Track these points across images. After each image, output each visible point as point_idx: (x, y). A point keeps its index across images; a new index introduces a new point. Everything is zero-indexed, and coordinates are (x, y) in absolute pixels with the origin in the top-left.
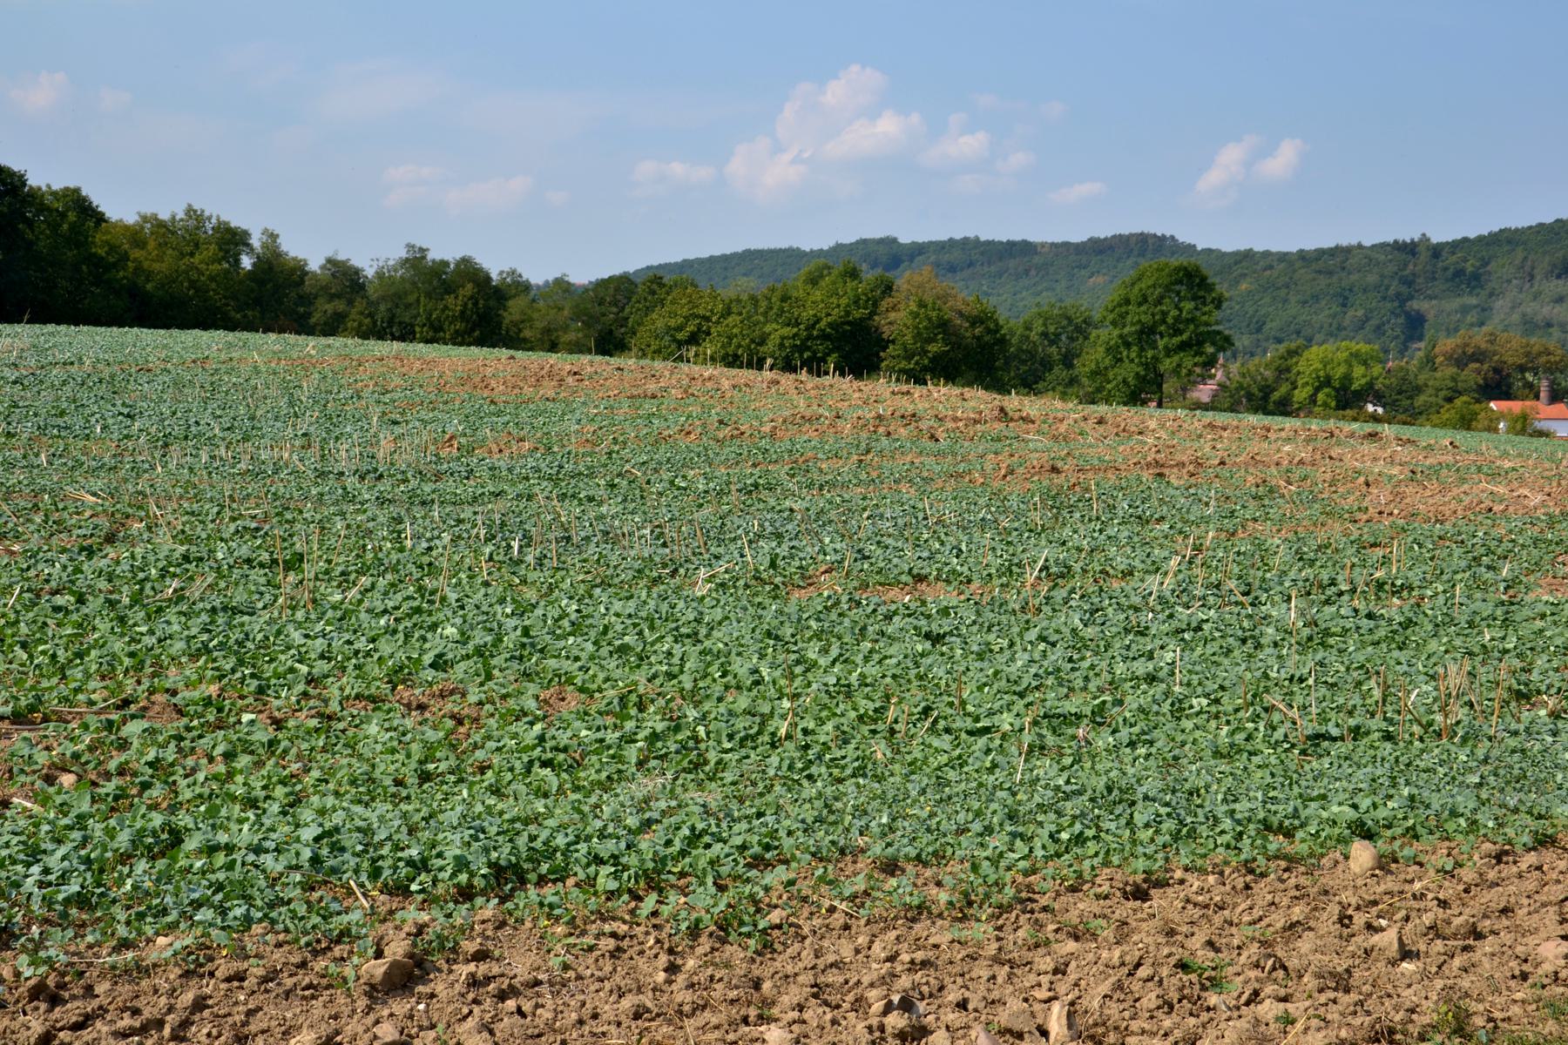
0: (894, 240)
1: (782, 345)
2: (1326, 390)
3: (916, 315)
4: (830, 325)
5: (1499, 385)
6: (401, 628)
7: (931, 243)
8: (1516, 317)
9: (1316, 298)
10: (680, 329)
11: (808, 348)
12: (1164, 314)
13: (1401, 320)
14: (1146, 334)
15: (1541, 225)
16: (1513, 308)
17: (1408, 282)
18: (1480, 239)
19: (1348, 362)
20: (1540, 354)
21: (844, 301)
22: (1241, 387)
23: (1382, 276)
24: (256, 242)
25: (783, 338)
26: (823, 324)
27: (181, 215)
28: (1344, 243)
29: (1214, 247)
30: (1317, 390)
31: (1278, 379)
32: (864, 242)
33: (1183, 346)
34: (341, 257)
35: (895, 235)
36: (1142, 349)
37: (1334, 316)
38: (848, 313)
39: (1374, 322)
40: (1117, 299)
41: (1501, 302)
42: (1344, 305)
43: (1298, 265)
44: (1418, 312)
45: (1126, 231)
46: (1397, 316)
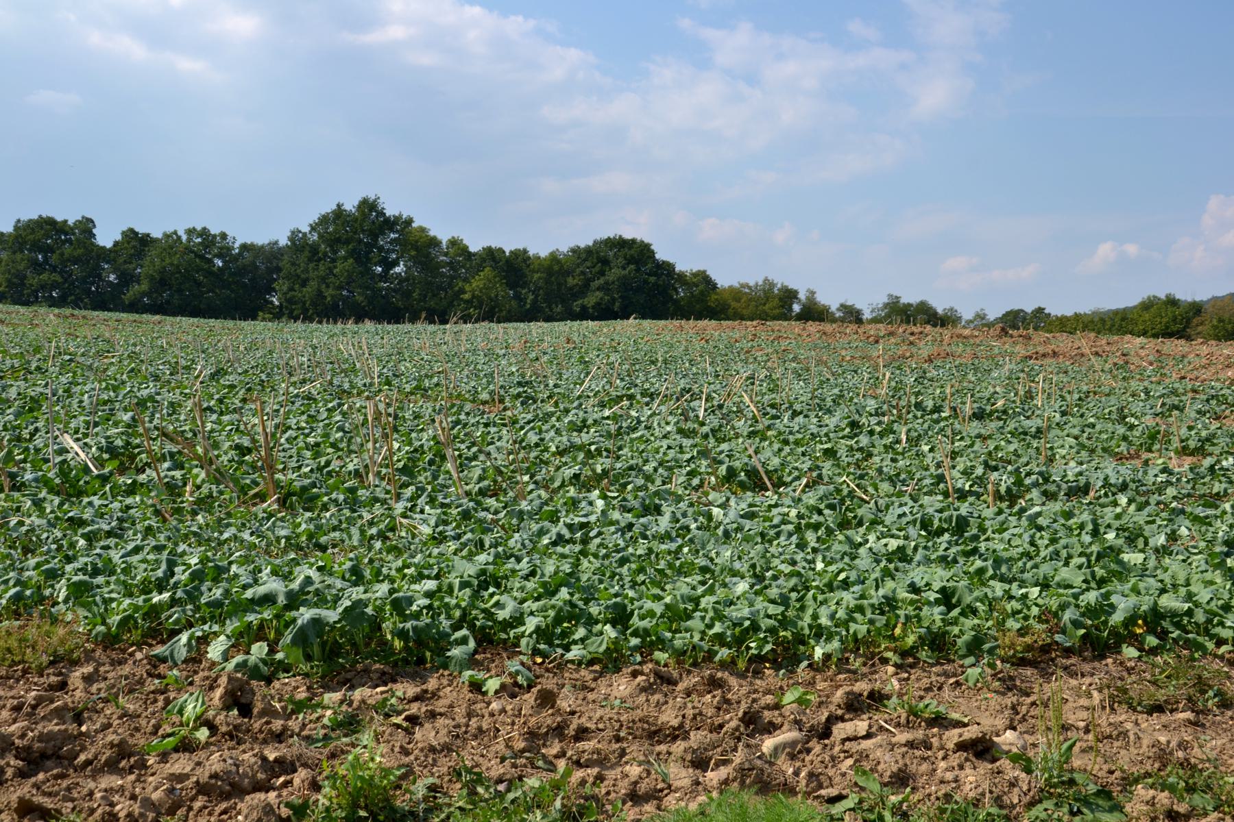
21: (1164, 320)
24: (802, 296)
27: (760, 283)
34: (849, 303)
38: (1167, 327)
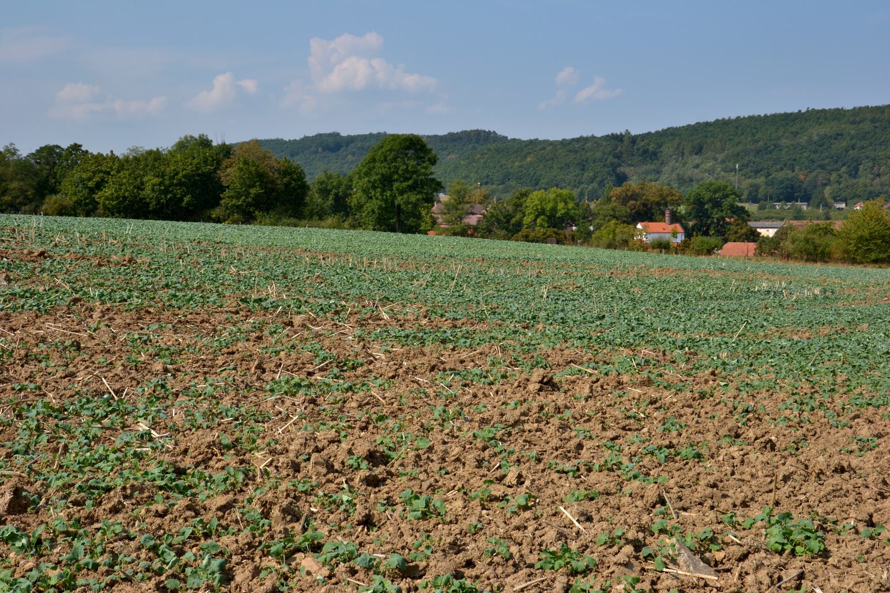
0: (338, 134)
1: (153, 190)
2: (542, 217)
3: (241, 170)
4: (184, 176)
5: (646, 213)
6: (480, 298)
7: (359, 136)
8: (674, 176)
9: (568, 166)
10: (90, 179)
11: (171, 192)
12: (397, 168)
13: (614, 178)
14: (386, 181)
15: (689, 125)
16: (673, 171)
17: (618, 156)
18: (657, 133)
19: (555, 200)
20: (667, 195)
22: (493, 216)
23: (604, 153)
25: (154, 185)
26: (180, 175)
28: (585, 135)
29: (517, 138)
30: (537, 217)
31: (515, 211)
32: (320, 135)
33: (412, 188)
35: (338, 131)
36: (384, 191)
37: (577, 176)
38: (198, 169)
39: (599, 179)
40: (368, 158)
41: (666, 168)
42: (583, 170)
43: (559, 147)
44: (624, 173)
45: (468, 129)
46: (611, 175)
